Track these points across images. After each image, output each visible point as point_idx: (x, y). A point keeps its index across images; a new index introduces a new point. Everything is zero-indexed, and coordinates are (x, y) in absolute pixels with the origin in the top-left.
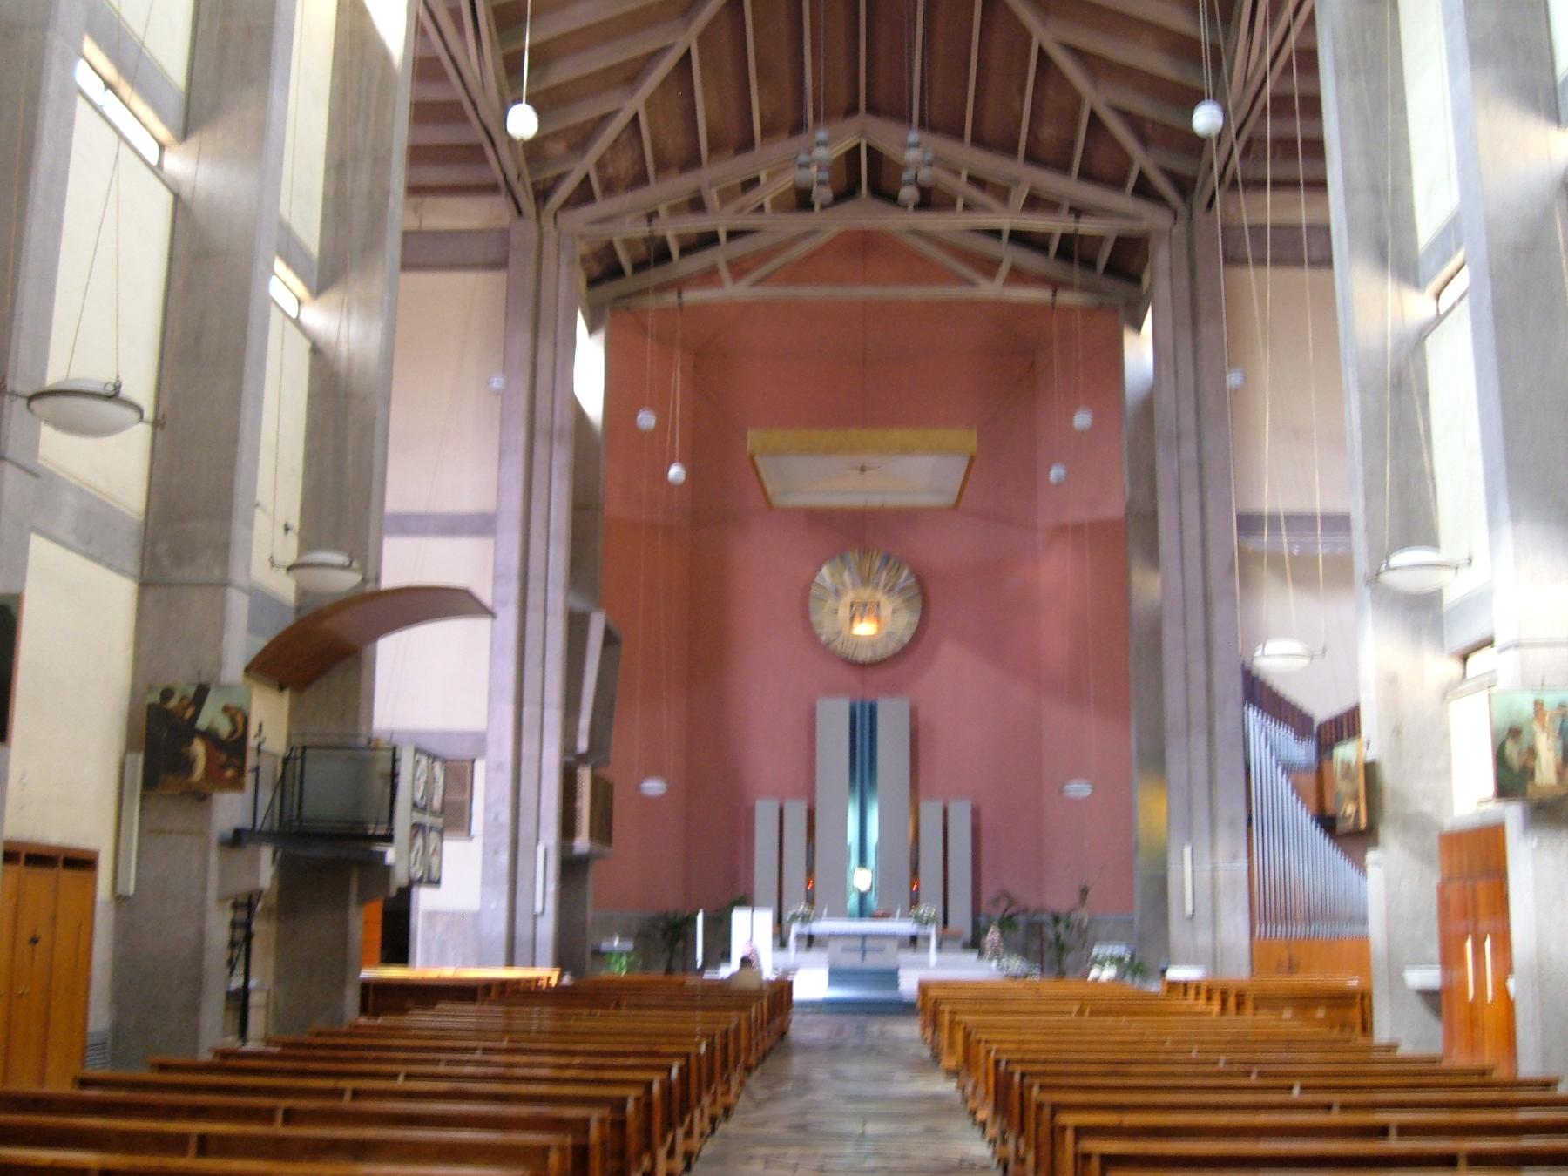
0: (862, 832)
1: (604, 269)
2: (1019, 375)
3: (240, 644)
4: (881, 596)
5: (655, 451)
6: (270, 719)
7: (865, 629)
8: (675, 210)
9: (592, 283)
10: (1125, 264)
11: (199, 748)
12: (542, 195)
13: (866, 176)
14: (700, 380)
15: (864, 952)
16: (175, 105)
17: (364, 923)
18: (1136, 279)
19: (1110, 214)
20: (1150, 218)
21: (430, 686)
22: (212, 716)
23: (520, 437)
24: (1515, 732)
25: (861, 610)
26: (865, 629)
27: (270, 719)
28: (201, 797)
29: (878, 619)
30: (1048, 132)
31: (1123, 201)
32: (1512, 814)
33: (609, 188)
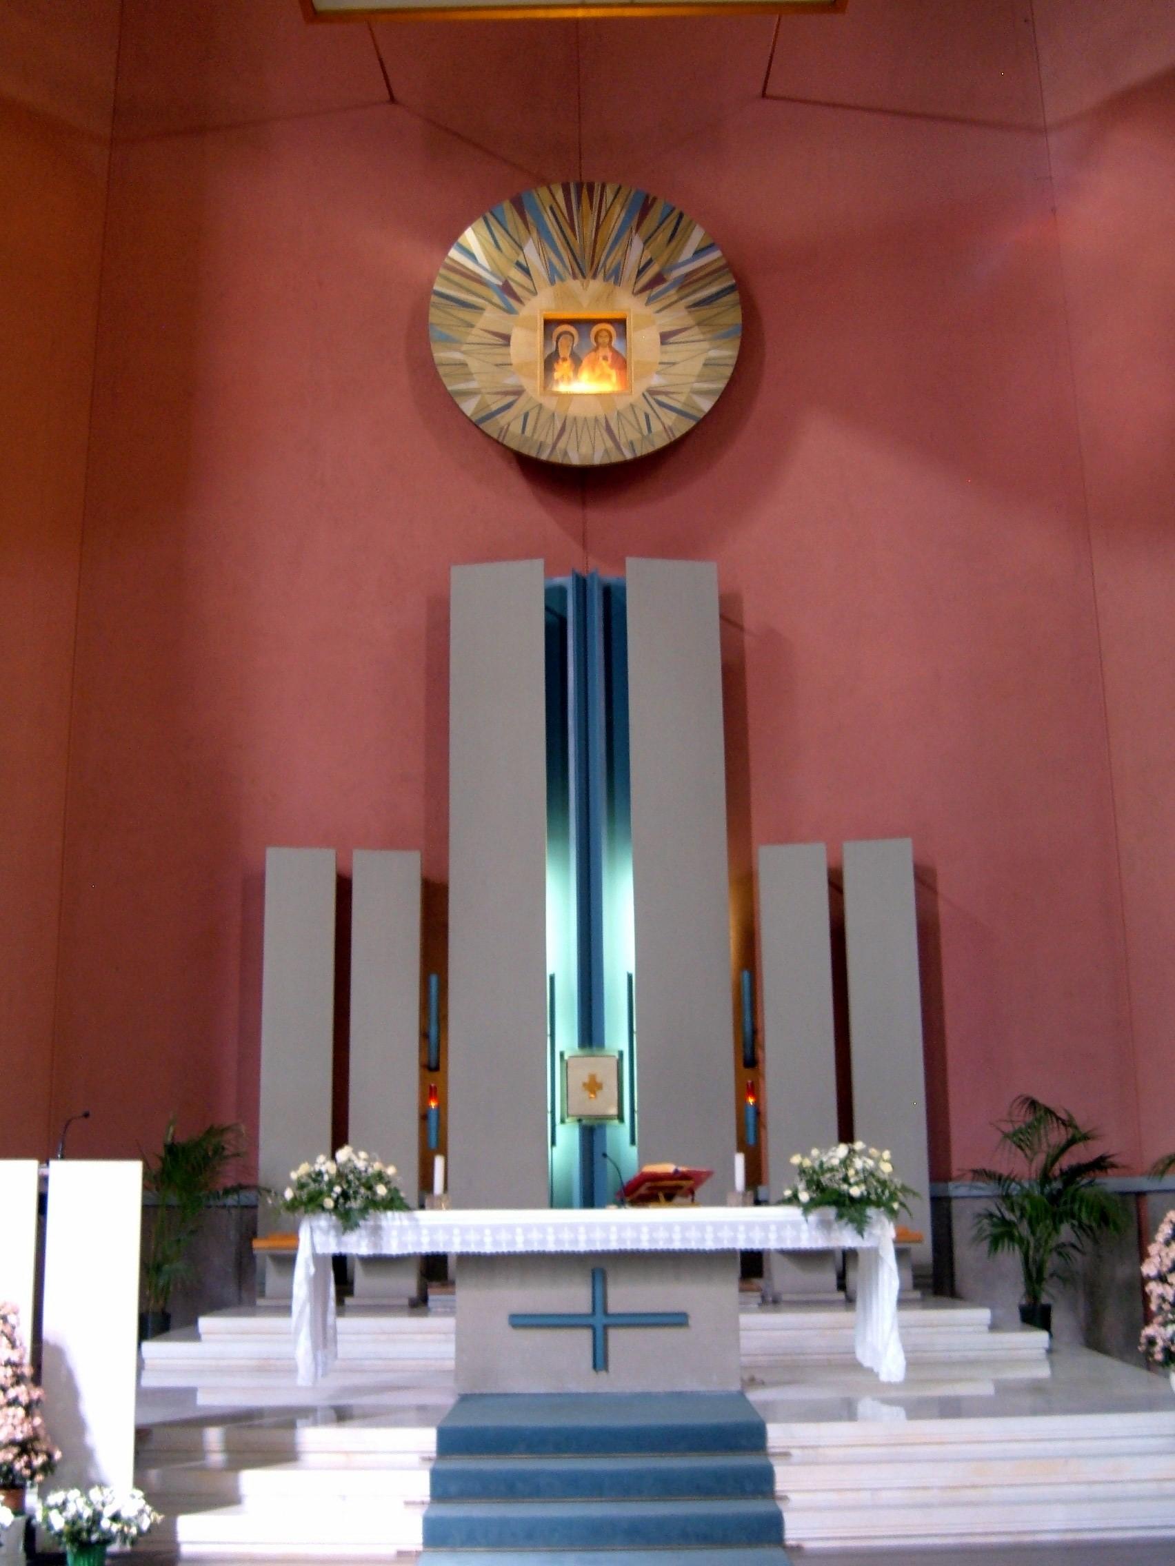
0: (589, 939)
4: (627, 304)
7: (587, 382)
15: (600, 1325)
25: (567, 336)
29: (621, 363)
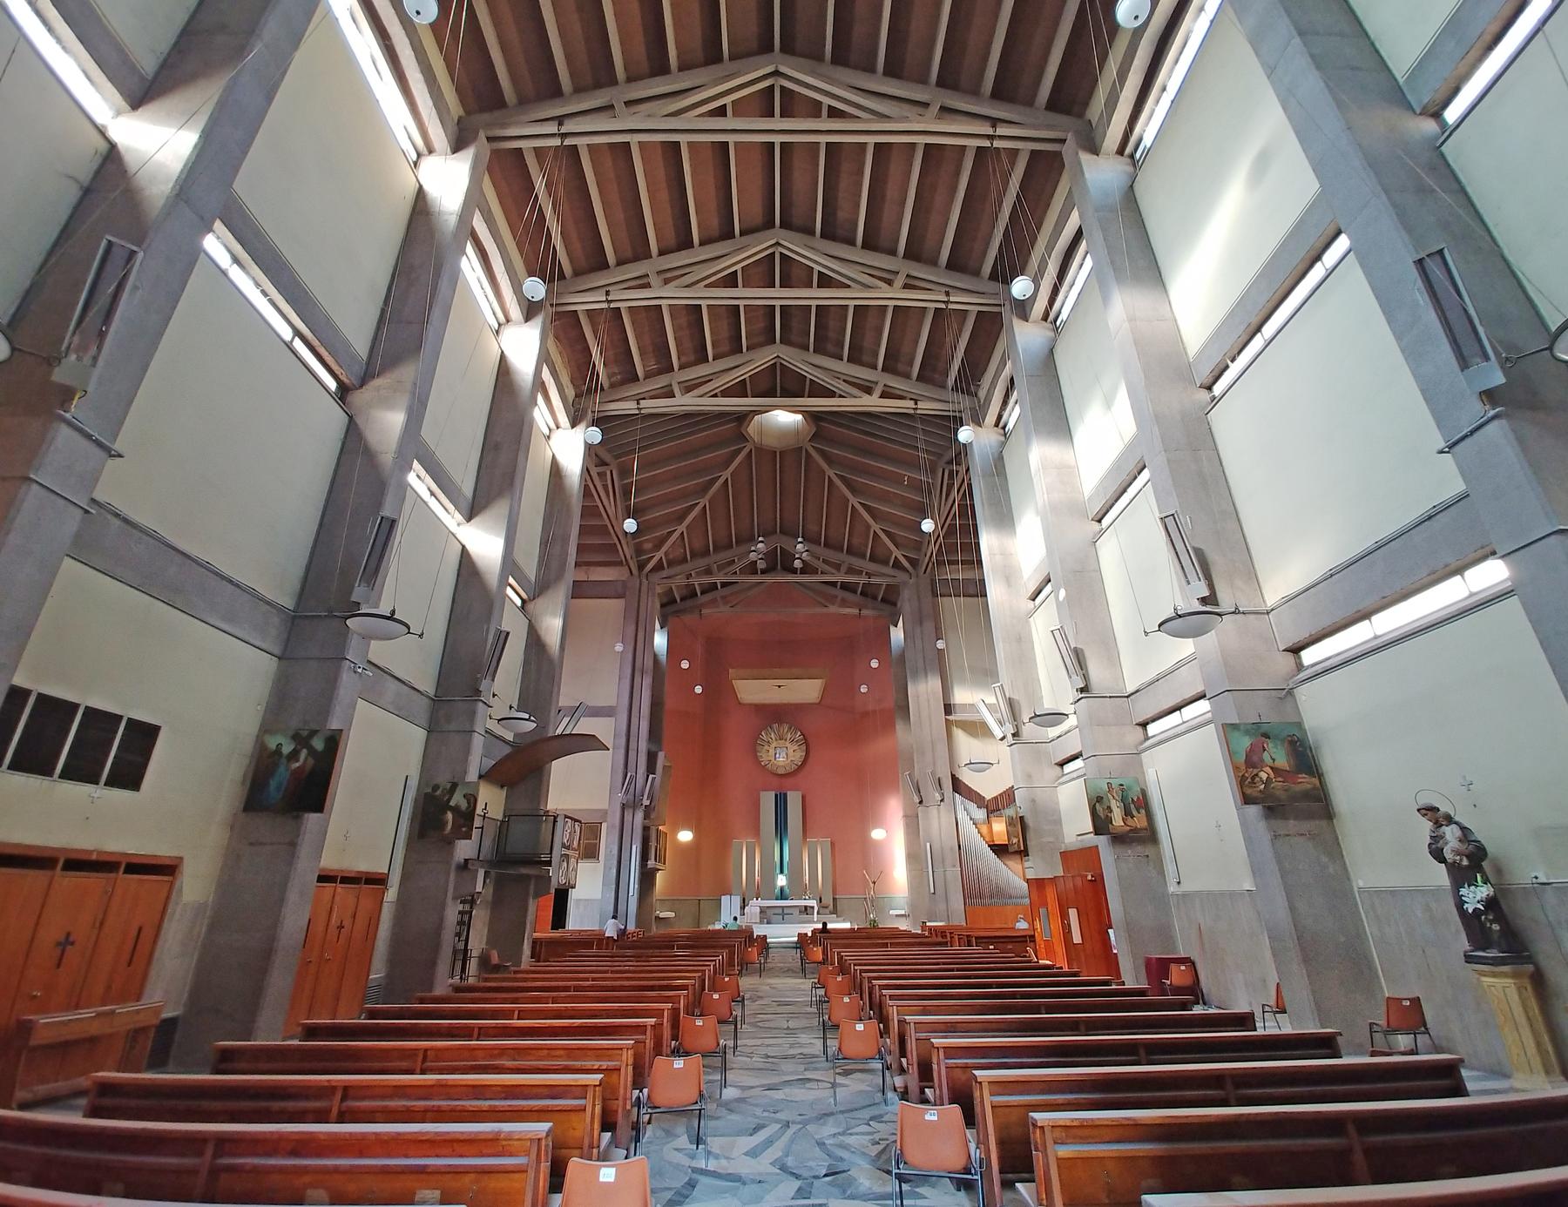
1: (668, 603)
2: (843, 651)
3: (477, 760)
5: (687, 679)
6: (491, 801)
8: (698, 574)
9: (662, 606)
10: (889, 601)
11: (450, 816)
12: (641, 567)
13: (780, 561)
14: (715, 658)
16: (465, 505)
17: (538, 910)
18: (895, 604)
19: (882, 578)
20: (901, 577)
21: (578, 786)
22: (458, 799)
23: (629, 671)
24: (1099, 799)
26: (781, 759)
27: (491, 801)
28: (449, 843)
30: (856, 541)
31: (888, 570)
32: (1102, 841)
33: (671, 564)
